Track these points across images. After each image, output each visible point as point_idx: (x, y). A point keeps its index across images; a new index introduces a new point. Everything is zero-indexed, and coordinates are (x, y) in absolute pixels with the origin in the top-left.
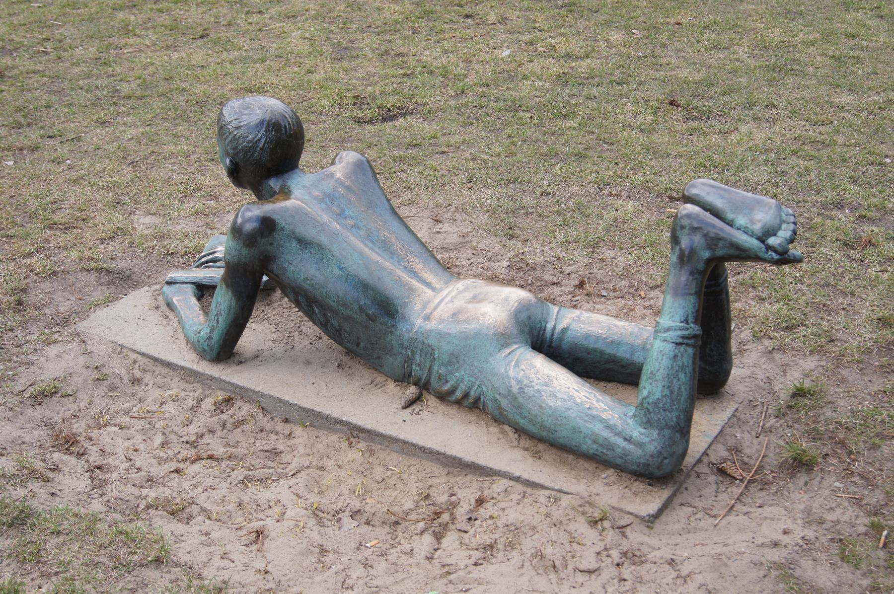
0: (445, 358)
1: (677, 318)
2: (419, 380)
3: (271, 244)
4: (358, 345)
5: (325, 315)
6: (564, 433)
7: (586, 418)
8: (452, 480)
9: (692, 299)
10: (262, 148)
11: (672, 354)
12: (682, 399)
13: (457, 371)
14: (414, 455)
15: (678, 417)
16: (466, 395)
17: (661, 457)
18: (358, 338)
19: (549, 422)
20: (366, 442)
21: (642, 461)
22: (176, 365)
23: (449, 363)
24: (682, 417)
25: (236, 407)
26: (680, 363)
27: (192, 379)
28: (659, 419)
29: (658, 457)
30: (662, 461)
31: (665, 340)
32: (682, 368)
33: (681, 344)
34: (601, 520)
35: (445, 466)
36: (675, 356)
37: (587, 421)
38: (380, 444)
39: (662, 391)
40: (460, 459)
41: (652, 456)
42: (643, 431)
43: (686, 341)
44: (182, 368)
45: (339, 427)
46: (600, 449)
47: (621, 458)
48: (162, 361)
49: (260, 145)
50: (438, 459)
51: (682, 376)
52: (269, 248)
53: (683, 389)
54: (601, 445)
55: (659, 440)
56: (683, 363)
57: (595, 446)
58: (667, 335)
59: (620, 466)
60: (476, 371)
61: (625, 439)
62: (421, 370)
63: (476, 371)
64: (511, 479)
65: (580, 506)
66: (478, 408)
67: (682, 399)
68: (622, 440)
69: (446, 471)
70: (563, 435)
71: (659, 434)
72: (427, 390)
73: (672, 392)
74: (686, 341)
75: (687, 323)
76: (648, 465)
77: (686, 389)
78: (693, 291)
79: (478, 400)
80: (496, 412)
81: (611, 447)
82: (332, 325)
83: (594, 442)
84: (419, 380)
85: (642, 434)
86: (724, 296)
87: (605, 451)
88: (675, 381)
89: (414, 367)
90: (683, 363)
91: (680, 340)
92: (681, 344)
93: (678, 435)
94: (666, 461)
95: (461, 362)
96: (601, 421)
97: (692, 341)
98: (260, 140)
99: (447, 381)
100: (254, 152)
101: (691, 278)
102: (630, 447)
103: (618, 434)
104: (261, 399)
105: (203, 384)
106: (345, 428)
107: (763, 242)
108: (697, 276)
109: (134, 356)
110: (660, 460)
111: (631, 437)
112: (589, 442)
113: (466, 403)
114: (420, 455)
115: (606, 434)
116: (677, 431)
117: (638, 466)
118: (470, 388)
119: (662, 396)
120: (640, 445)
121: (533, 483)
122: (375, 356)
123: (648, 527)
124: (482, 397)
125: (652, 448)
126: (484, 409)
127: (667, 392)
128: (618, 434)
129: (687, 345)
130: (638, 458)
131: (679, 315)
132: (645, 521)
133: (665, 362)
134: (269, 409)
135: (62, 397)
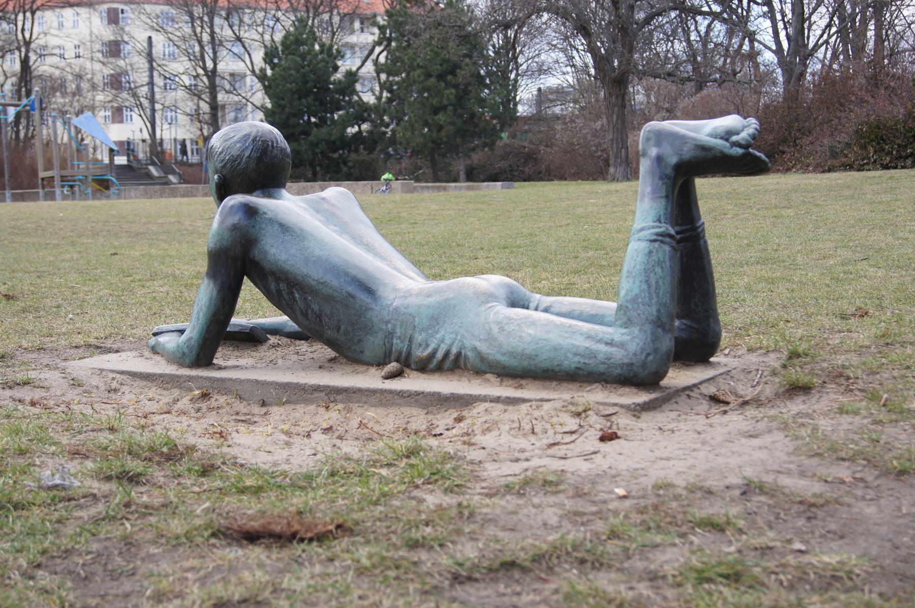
0: (426, 322)
1: (650, 218)
2: (400, 354)
3: (254, 227)
4: (339, 329)
5: (305, 299)
6: (545, 356)
7: (567, 335)
8: (430, 417)
9: (663, 202)
10: (249, 157)
11: (647, 250)
12: (661, 292)
13: (437, 332)
14: (393, 404)
15: (658, 311)
16: (447, 354)
17: (644, 354)
18: (339, 321)
19: (530, 349)
20: (344, 403)
21: (626, 361)
22: (155, 375)
23: (431, 326)
24: (662, 311)
25: (213, 400)
26: (655, 258)
27: (169, 386)
28: (639, 315)
29: (642, 353)
30: (646, 357)
31: (639, 240)
32: (659, 263)
33: (655, 241)
34: (585, 411)
35: (424, 406)
36: (650, 252)
37: (567, 338)
38: (358, 402)
39: (640, 286)
40: (439, 394)
41: (635, 354)
42: (624, 331)
43: (660, 238)
44: (161, 375)
45: (316, 395)
46: (582, 361)
47: (604, 363)
48: (141, 374)
49: (247, 154)
50: (416, 401)
51: (658, 270)
52: (251, 230)
53: (661, 283)
54: (583, 356)
55: (641, 336)
56: (659, 259)
57: (577, 359)
58: (642, 234)
59: (603, 374)
60: (457, 327)
61: (607, 344)
62: (402, 342)
63: (457, 327)
64: (491, 401)
65: (564, 407)
66: (459, 367)
67: (661, 292)
68: (603, 345)
69: (425, 411)
70: (545, 359)
71: (640, 330)
72: (408, 366)
73: (649, 287)
74: (660, 238)
75: (660, 222)
76: (632, 364)
77: (664, 283)
78: (664, 194)
79: (459, 354)
80: (477, 362)
81: (593, 355)
82: (313, 310)
83: (576, 354)
84: (400, 354)
85: (623, 334)
86: (702, 242)
87: (587, 361)
88: (652, 275)
89: (395, 341)
90: (659, 259)
91: (654, 237)
92: (655, 241)
93: (660, 330)
94: (650, 358)
95: (441, 323)
96: (581, 334)
97: (668, 239)
98: (247, 147)
99: (427, 345)
100: (242, 159)
101: (660, 182)
102: (613, 350)
103: (599, 341)
104: (238, 387)
105: (181, 388)
106: (323, 394)
107: (727, 140)
108: (666, 181)
109: (112, 375)
110: (643, 357)
111: (613, 340)
112: (570, 356)
113: (447, 364)
114: (398, 401)
115: (588, 344)
116: (659, 326)
117: (622, 368)
118: (451, 346)
119: (640, 291)
120: (622, 345)
121: (514, 398)
122: (357, 338)
123: (634, 416)
124: (463, 351)
125: (633, 347)
126: (465, 365)
127: (645, 287)
128: (599, 341)
129: (662, 242)
130: (621, 359)
131: (653, 214)
132: (631, 410)
133: (641, 258)
134: (245, 396)
135: (35, 387)
